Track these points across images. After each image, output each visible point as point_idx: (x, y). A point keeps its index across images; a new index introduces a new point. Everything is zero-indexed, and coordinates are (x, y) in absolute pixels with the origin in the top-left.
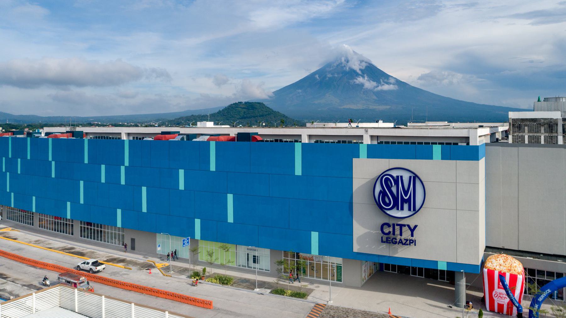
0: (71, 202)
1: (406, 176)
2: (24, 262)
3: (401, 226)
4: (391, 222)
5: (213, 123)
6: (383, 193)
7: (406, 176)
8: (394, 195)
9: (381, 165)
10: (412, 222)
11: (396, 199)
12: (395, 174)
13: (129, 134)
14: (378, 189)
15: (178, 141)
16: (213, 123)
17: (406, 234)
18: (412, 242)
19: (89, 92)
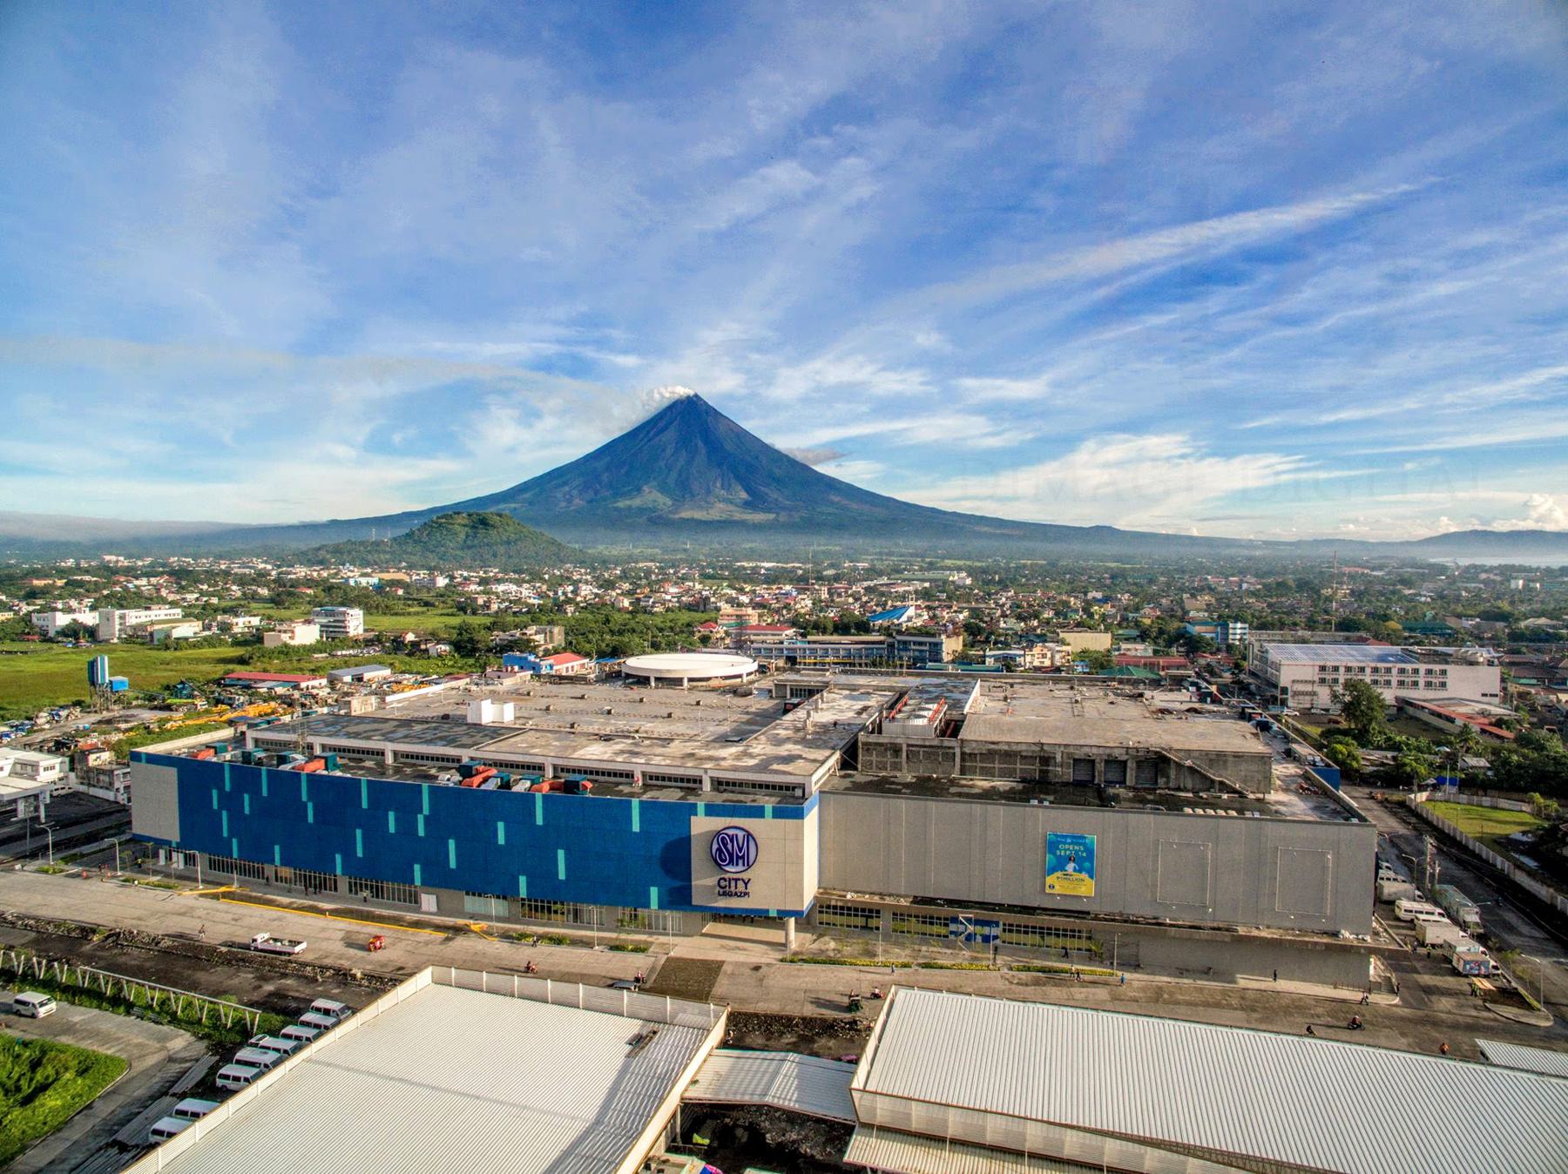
0: (396, 810)
1: (741, 834)
2: (333, 539)
3: (736, 880)
4: (727, 876)
5: (693, 818)
6: (719, 849)
7: (741, 834)
8: (731, 852)
9: (718, 823)
10: (745, 876)
11: (731, 855)
12: (730, 832)
13: (395, 753)
14: (715, 846)
15: (492, 792)
16: (693, 818)
17: (741, 885)
18: (746, 894)
19: (1077, 547)
